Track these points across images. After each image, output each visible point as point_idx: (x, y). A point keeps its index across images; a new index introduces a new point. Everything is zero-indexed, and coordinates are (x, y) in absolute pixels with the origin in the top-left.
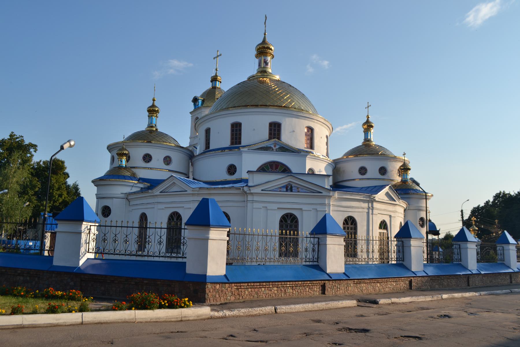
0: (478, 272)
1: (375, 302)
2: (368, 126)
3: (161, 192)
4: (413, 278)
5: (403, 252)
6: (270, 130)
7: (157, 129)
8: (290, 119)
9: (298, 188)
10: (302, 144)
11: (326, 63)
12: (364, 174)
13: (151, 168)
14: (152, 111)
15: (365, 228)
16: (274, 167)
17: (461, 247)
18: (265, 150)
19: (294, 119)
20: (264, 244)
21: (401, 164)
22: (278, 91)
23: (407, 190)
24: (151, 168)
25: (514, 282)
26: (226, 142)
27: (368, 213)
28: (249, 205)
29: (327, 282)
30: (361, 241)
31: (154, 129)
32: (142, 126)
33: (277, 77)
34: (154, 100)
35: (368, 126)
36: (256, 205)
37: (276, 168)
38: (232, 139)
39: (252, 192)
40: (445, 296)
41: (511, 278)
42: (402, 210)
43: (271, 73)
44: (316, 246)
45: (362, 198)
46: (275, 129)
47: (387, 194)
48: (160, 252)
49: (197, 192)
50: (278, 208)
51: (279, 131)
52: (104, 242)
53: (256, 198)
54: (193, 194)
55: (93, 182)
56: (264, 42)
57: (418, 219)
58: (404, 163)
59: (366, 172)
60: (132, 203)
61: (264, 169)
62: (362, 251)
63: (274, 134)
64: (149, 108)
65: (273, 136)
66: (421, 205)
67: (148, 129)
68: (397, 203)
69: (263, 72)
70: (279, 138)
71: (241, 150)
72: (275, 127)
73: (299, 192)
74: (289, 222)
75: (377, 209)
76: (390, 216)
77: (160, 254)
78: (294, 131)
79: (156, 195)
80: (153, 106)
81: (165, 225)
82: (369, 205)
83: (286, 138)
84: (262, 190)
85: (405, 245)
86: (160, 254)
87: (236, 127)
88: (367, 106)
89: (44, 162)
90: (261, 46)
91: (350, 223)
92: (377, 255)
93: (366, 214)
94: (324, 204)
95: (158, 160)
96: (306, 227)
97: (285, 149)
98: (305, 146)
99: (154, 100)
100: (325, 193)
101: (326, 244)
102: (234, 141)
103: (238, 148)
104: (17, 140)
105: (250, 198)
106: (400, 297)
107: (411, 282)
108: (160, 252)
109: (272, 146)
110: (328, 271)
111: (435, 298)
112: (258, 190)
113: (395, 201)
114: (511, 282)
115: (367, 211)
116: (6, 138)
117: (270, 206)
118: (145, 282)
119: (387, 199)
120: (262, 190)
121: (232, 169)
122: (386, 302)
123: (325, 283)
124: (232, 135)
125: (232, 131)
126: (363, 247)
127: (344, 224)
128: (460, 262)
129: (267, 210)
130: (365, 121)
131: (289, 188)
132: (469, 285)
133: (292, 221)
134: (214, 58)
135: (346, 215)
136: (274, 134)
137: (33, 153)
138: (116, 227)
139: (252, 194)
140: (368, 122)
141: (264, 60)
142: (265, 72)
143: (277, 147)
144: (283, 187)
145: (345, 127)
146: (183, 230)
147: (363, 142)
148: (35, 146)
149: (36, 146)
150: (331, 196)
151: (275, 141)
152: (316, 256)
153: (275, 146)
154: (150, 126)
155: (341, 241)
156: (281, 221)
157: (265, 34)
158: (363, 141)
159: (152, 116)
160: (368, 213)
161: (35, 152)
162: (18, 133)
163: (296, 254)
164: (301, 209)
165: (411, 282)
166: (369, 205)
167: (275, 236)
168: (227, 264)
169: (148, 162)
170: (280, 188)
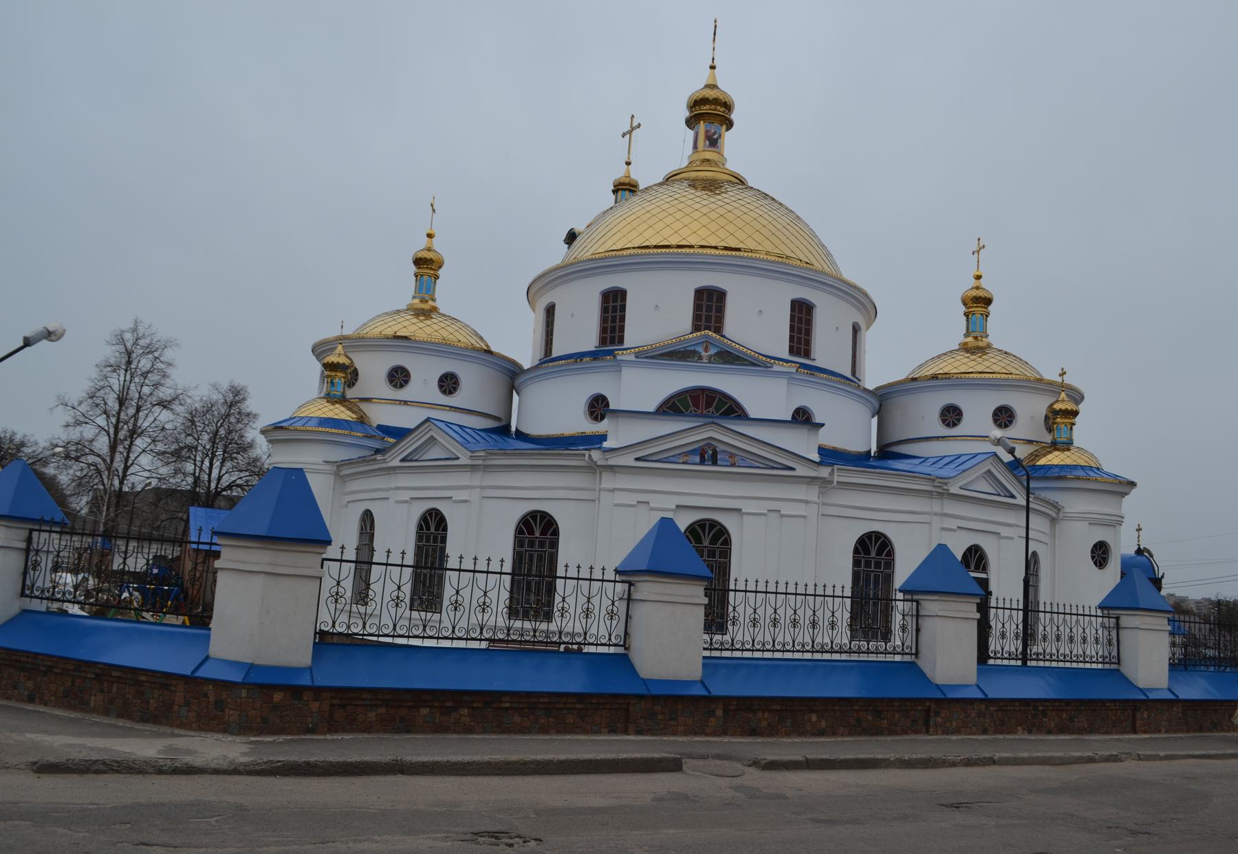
3: (403, 460)
6: (697, 307)
9: (732, 455)
12: (955, 425)
13: (405, 403)
16: (702, 403)
24: (405, 403)
26: (588, 339)
37: (708, 406)
38: (603, 330)
44: (1114, 633)
48: (334, 623)
49: (480, 462)
50: (678, 506)
51: (721, 310)
52: (336, 601)
54: (473, 468)
55: (1132, 484)
59: (959, 420)
61: (673, 407)
63: (708, 319)
65: (703, 323)
72: (710, 299)
73: (733, 465)
77: (394, 629)
79: (393, 469)
81: (410, 559)
84: (637, 459)
86: (394, 629)
87: (710, 299)
97: (730, 358)
102: (609, 335)
103: (611, 353)
105: (608, 481)
108: (334, 623)
109: (700, 349)
113: (1013, 497)
118: (114, 674)
120: (637, 459)
121: (598, 407)
124: (604, 320)
125: (605, 310)
131: (708, 455)
133: (879, 553)
136: (708, 319)
138: (341, 561)
143: (712, 351)
144: (692, 452)
146: (732, 594)
151: (707, 336)
152: (1114, 653)
153: (706, 351)
156: (519, 531)
163: (886, 635)
169: (402, 386)
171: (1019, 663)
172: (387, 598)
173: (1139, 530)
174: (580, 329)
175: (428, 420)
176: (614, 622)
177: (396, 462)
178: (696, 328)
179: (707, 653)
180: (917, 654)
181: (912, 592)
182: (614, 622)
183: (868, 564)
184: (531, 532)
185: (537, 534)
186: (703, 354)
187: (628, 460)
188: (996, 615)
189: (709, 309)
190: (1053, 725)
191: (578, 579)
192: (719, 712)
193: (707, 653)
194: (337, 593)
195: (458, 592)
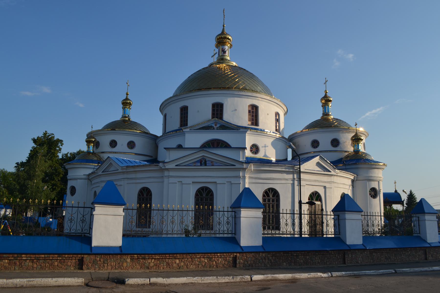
0: (364, 248)
1: (122, 282)
2: (326, 100)
3: (103, 172)
4: (238, 255)
5: (339, 225)
6: (213, 110)
7: (129, 119)
8: (232, 99)
9: (212, 162)
10: (244, 120)
11: (351, 56)
12: (317, 147)
14: (126, 103)
15: (290, 200)
17: (340, 218)
18: (206, 129)
19: (236, 99)
20: (366, 222)
21: (353, 134)
22: (230, 74)
23: (354, 162)
25: (430, 258)
27: (293, 185)
28: (166, 180)
29: (86, 256)
30: (285, 215)
31: (127, 119)
32: (117, 116)
33: (234, 64)
34: (127, 94)
35: (326, 100)
36: (171, 180)
38: (181, 121)
39: (167, 167)
40: (256, 277)
41: (426, 254)
42: (350, 182)
43: (229, 61)
45: (284, 170)
46: (218, 109)
47: (318, 164)
48: (70, 229)
49: (125, 171)
52: (71, 222)
53: (172, 173)
54: (123, 173)
56: (223, 33)
57: (368, 190)
58: (356, 133)
59: (318, 145)
60: (93, 182)
62: (287, 224)
63: (217, 114)
64: (123, 100)
66: (371, 175)
67: (123, 119)
68: (333, 173)
69: (222, 60)
70: (221, 118)
71: (184, 130)
73: (213, 165)
74: (205, 196)
75: (305, 180)
76: (325, 187)
77: (82, 231)
78: (236, 110)
80: (127, 99)
82: (294, 176)
83: (227, 116)
84: (176, 166)
85: (420, 220)
88: (325, 82)
89: (70, 154)
90: (220, 36)
91: (272, 195)
92: (306, 229)
93: (290, 186)
94: (239, 177)
95: (122, 145)
96: (222, 201)
97: (228, 127)
98: (250, 123)
99: (127, 94)
100: (238, 166)
101: (240, 217)
104: (50, 137)
105: (166, 173)
106: (168, 277)
107: (235, 259)
108: (70, 229)
109: (213, 125)
110: (348, 243)
111: (238, 279)
112: (172, 166)
113: (330, 171)
114: (426, 259)
115: (292, 182)
116: (40, 136)
117: (185, 181)
119: (319, 169)
120: (176, 166)
122: (140, 283)
123: (83, 257)
126: (289, 221)
127: (264, 196)
128: (418, 235)
129: (183, 184)
130: (324, 96)
132: (345, 263)
133: (207, 195)
134: (212, 57)
135: (266, 187)
136: (217, 114)
137: (61, 147)
139: (168, 169)
140: (326, 96)
141: (222, 49)
142: (222, 59)
143: (218, 126)
145: (374, 111)
147: (322, 117)
148: (61, 141)
149: (62, 141)
150: (246, 169)
153: (216, 125)
154: (124, 117)
155: (258, 213)
157: (224, 26)
158: (322, 115)
159: (125, 108)
160: (293, 185)
161: (62, 146)
162: (49, 132)
164: (216, 182)
165: (235, 259)
166: (294, 176)
167: (192, 211)
168: (124, 236)
169: (114, 147)
170: (195, 163)
171: (184, 236)
172: (79, 220)
173: (395, 183)
174: (175, 123)
175: (109, 157)
176: (72, 224)
177: (100, 173)
178: (213, 117)
179: (263, 236)
180: (235, 234)
181: (234, 208)
182: (229, 226)
183: (269, 200)
184: (143, 195)
185: (145, 196)
186: (215, 127)
187: (172, 166)
188: (283, 217)
189: (217, 110)
190: (302, 261)
191: (78, 207)
192: (129, 260)
193: (263, 236)
194: (71, 219)
195: (83, 216)
